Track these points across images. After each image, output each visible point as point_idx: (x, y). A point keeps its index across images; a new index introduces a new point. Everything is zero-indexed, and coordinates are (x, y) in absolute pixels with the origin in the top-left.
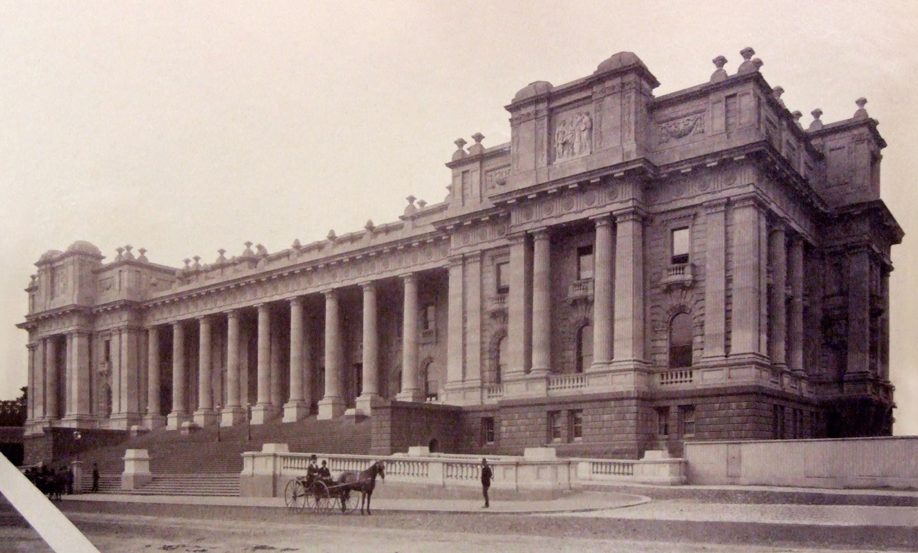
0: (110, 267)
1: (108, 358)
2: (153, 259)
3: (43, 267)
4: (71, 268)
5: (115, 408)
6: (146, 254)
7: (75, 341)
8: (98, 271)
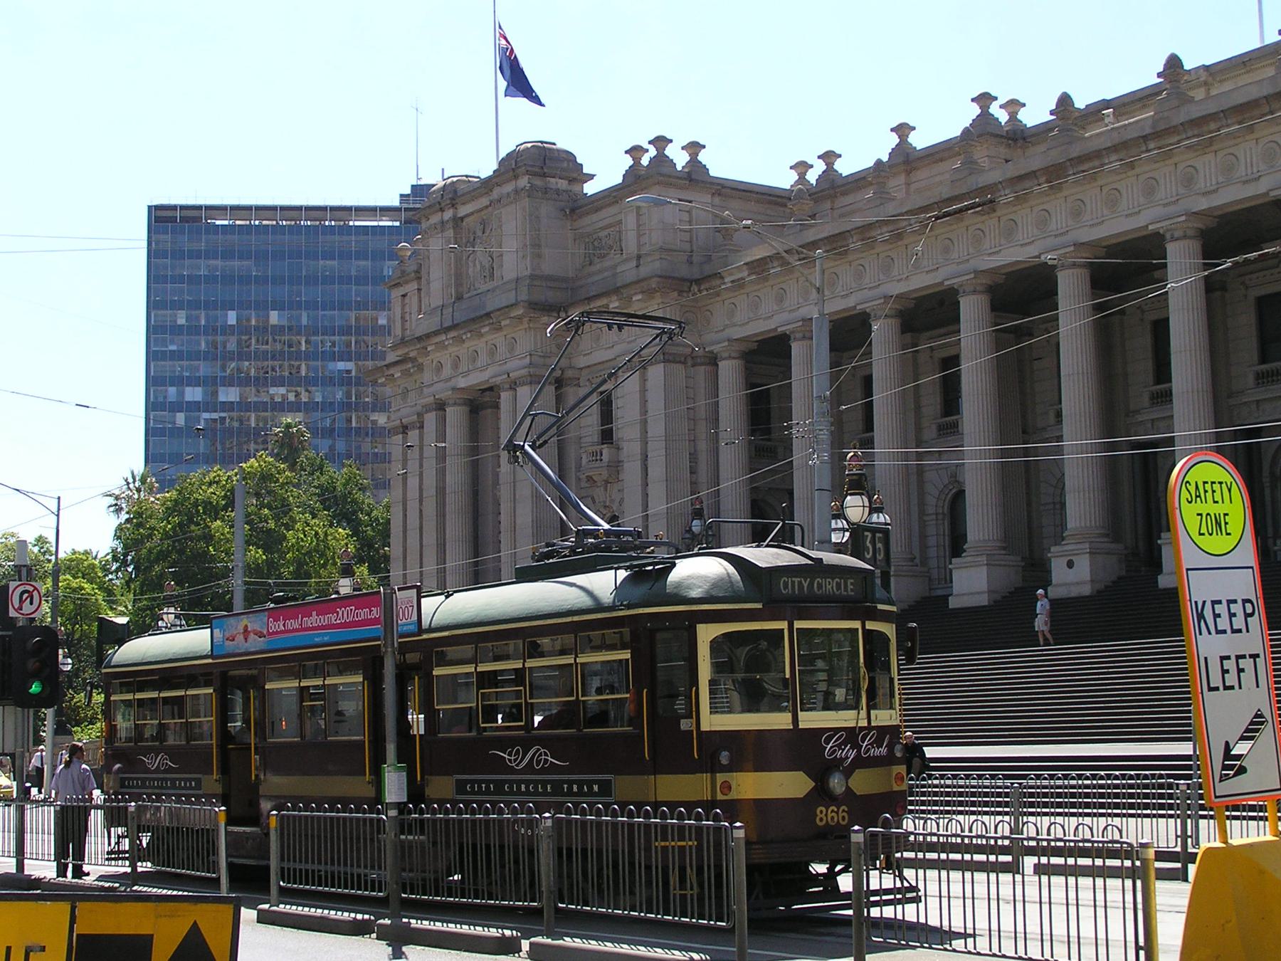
2: (719, 165)
6: (703, 157)
8: (577, 207)
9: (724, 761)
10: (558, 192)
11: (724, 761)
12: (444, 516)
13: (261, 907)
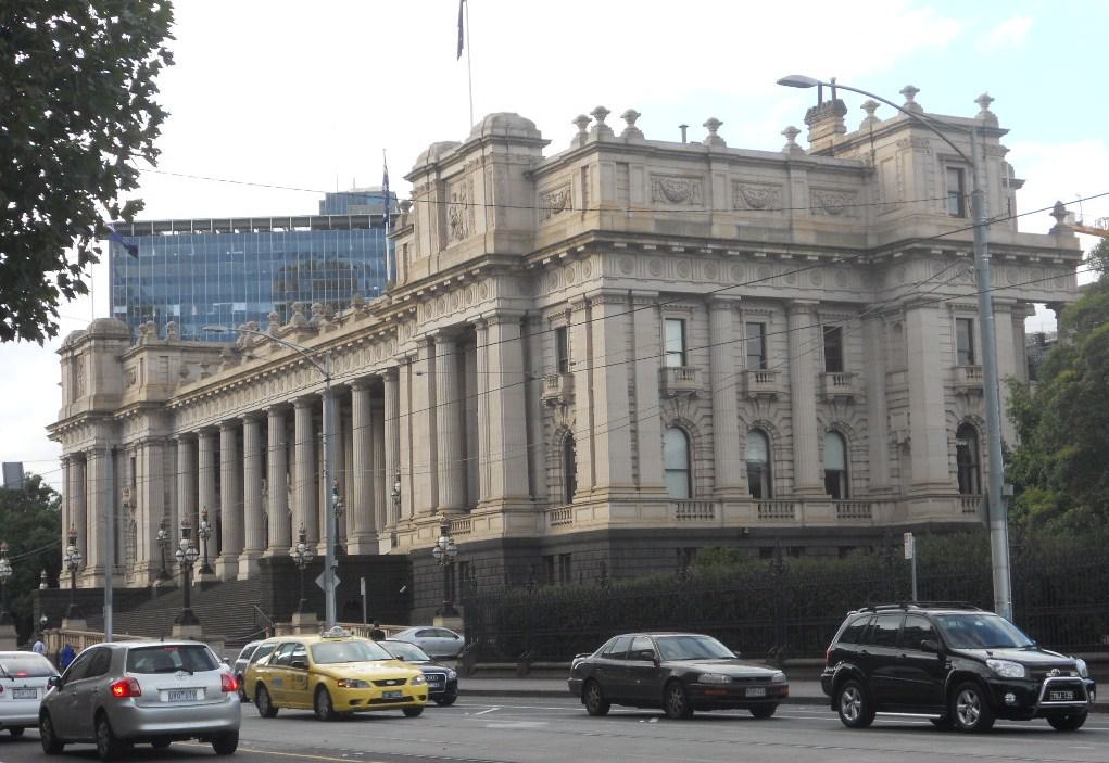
0: (565, 161)
1: (563, 365)
3: (423, 181)
4: (478, 177)
5: (583, 478)
7: (495, 332)
8: (533, 175)
9: (909, 543)
10: (113, 347)
11: (909, 543)
12: (464, 387)
13: (578, 661)
